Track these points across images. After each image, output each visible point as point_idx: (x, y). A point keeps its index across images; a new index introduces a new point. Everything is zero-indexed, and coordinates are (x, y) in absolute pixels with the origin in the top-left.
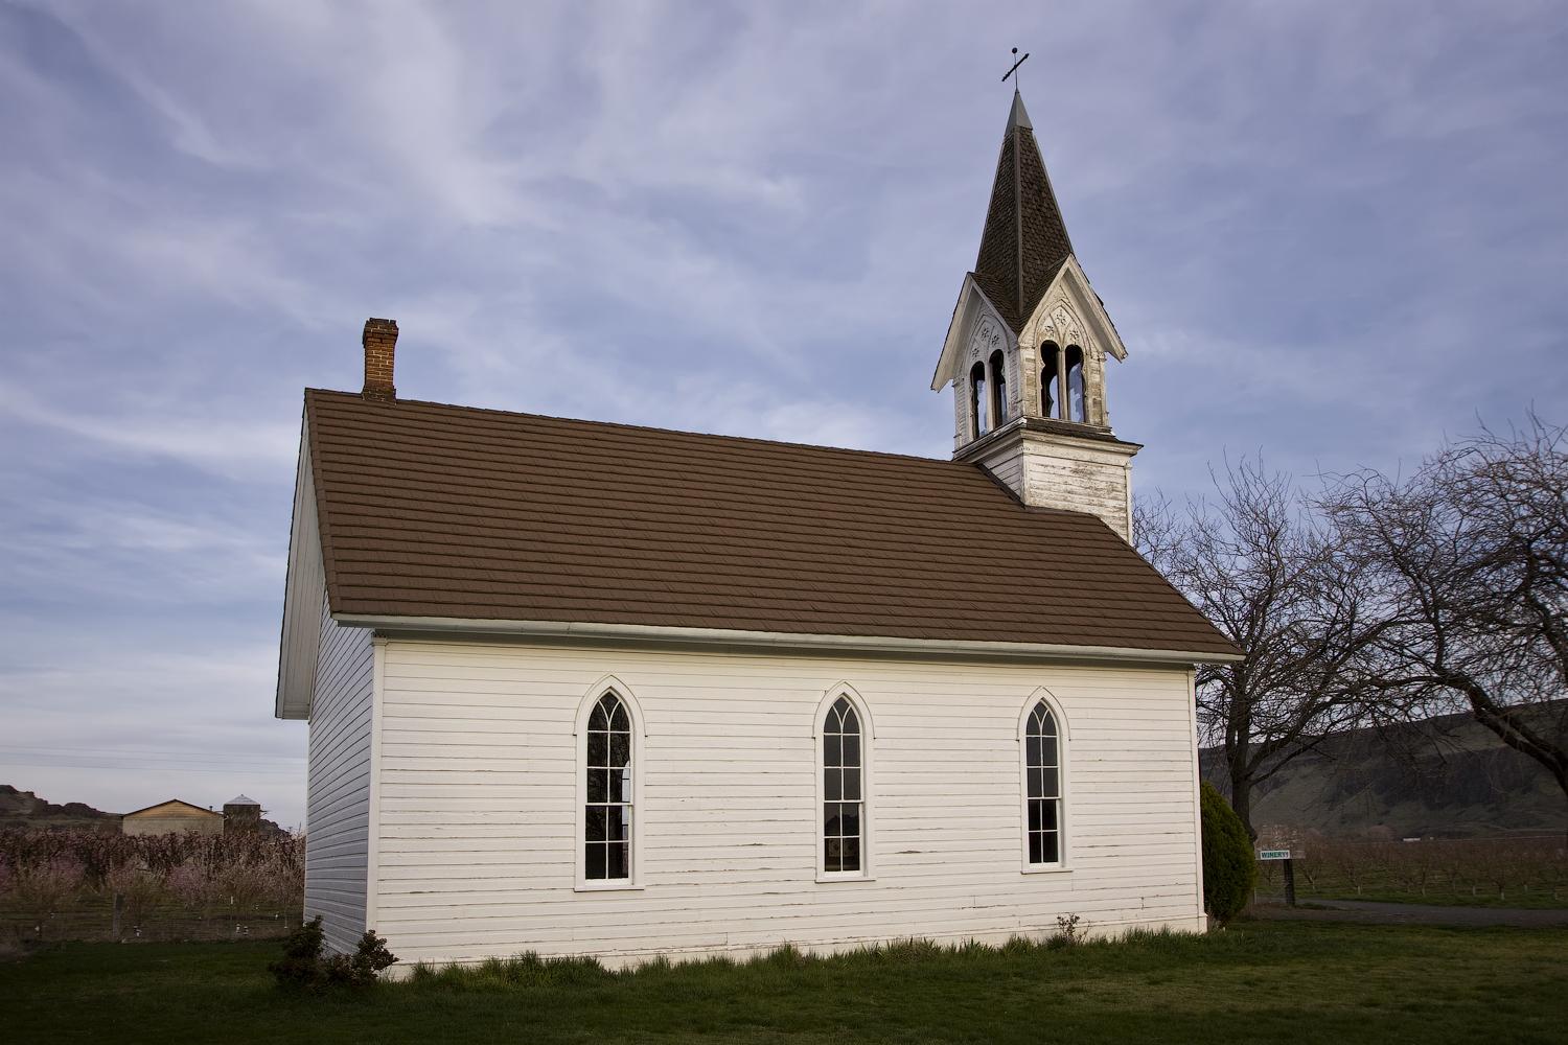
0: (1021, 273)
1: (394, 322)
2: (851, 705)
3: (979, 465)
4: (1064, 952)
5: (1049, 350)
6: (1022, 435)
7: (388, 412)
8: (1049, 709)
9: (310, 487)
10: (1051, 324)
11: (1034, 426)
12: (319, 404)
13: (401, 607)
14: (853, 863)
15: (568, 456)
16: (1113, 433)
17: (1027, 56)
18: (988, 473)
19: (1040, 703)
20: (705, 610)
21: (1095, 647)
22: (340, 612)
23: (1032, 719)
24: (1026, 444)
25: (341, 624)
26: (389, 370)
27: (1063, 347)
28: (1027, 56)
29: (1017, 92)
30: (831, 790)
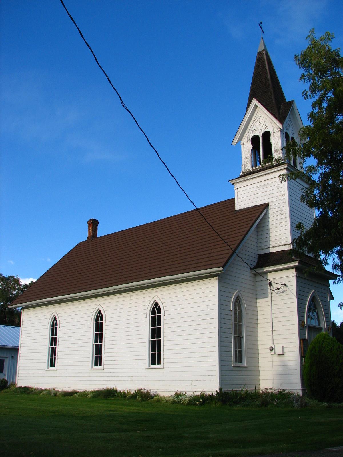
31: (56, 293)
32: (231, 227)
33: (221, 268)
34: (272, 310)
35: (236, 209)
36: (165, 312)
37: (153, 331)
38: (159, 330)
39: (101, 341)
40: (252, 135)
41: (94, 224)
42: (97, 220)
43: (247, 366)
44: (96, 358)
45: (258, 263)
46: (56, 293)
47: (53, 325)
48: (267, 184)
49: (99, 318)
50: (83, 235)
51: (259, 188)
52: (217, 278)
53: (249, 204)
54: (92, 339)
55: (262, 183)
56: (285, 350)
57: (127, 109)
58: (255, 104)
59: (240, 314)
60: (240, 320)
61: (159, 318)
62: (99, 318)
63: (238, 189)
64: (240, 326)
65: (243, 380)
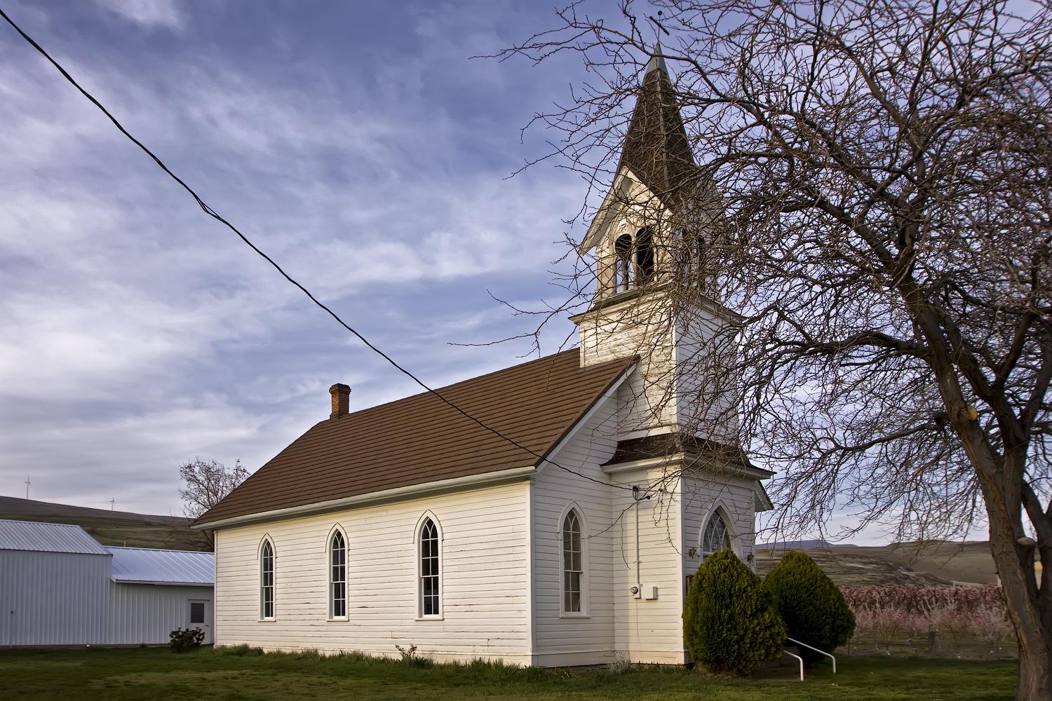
31: (243, 509)
32: (566, 397)
33: (533, 468)
34: (638, 530)
35: (582, 366)
36: (444, 535)
37: (425, 563)
38: (435, 562)
39: (343, 578)
41: (341, 392)
43: (589, 616)
44: (337, 603)
45: (617, 454)
46: (243, 509)
47: (266, 554)
49: (338, 542)
50: (325, 412)
52: (528, 482)
54: (328, 575)
56: (660, 592)
57: (218, 218)
59: (577, 537)
60: (577, 546)
61: (435, 543)
62: (338, 542)
63: (585, 331)
64: (577, 557)
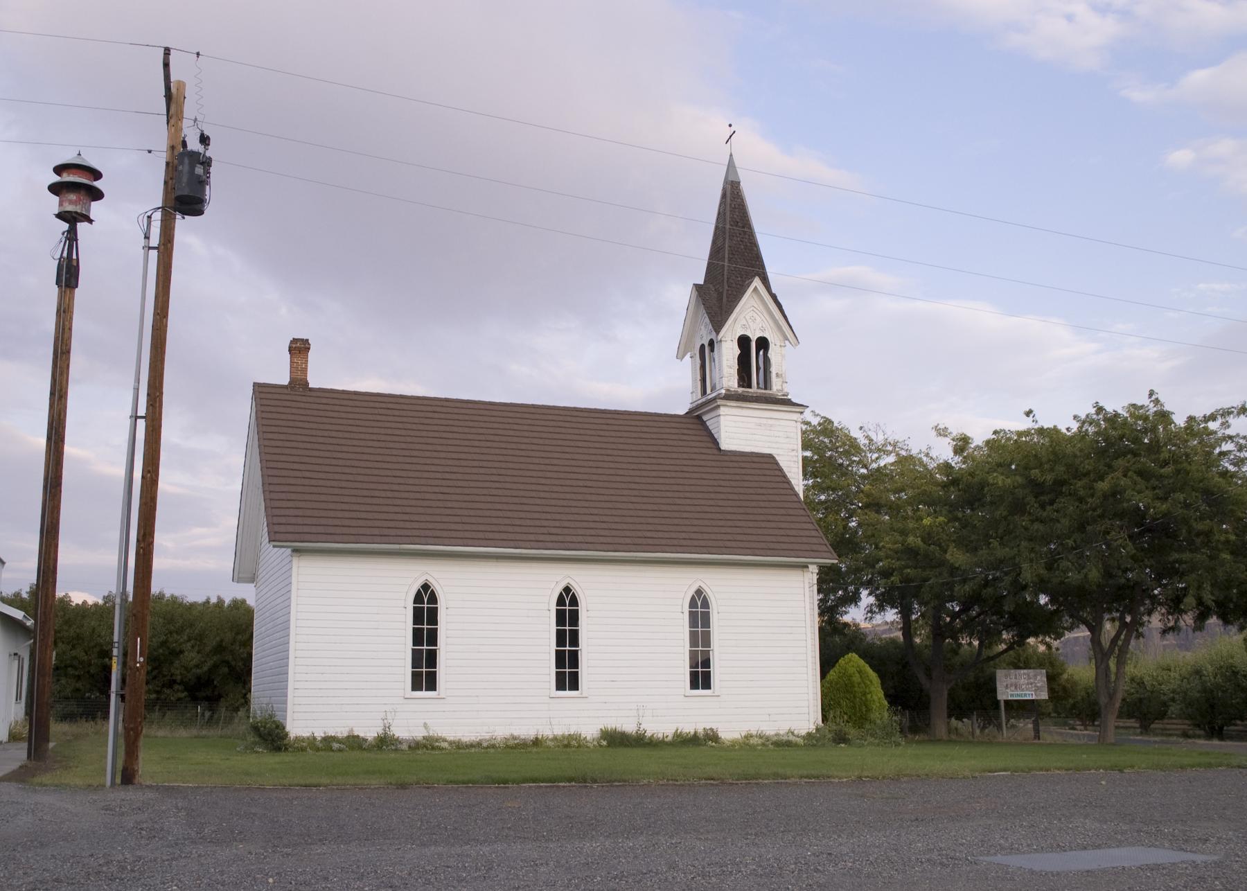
0: (726, 287)
1: (307, 340)
2: (573, 590)
3: (699, 417)
4: (704, 741)
5: (744, 342)
6: (719, 403)
7: (304, 399)
8: (704, 593)
9: (256, 451)
10: (745, 323)
11: (730, 397)
12: (262, 392)
13: (307, 537)
14: (574, 686)
15: (414, 427)
16: (789, 397)
17: (734, 132)
18: (703, 423)
19: (699, 589)
20: (481, 535)
21: (710, 555)
22: (274, 541)
23: (693, 599)
24: (722, 408)
25: (274, 546)
26: (305, 371)
27: (754, 339)
28: (734, 132)
29: (731, 155)
30: (694, 641)
40: (740, 332)
42: (771, 456)
48: (771, 426)
51: (759, 427)
53: (742, 447)
55: (764, 421)
58: (756, 287)
65: (278, 689)
